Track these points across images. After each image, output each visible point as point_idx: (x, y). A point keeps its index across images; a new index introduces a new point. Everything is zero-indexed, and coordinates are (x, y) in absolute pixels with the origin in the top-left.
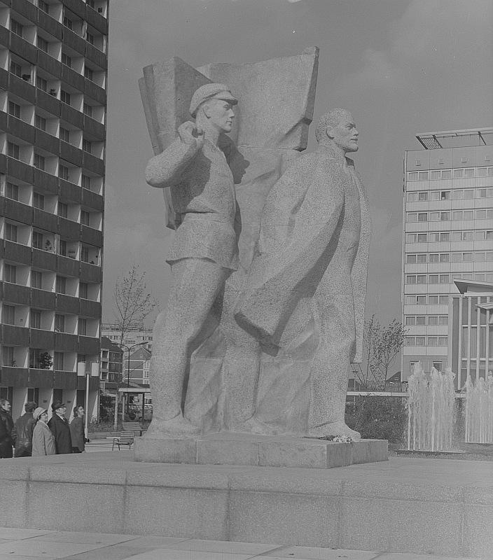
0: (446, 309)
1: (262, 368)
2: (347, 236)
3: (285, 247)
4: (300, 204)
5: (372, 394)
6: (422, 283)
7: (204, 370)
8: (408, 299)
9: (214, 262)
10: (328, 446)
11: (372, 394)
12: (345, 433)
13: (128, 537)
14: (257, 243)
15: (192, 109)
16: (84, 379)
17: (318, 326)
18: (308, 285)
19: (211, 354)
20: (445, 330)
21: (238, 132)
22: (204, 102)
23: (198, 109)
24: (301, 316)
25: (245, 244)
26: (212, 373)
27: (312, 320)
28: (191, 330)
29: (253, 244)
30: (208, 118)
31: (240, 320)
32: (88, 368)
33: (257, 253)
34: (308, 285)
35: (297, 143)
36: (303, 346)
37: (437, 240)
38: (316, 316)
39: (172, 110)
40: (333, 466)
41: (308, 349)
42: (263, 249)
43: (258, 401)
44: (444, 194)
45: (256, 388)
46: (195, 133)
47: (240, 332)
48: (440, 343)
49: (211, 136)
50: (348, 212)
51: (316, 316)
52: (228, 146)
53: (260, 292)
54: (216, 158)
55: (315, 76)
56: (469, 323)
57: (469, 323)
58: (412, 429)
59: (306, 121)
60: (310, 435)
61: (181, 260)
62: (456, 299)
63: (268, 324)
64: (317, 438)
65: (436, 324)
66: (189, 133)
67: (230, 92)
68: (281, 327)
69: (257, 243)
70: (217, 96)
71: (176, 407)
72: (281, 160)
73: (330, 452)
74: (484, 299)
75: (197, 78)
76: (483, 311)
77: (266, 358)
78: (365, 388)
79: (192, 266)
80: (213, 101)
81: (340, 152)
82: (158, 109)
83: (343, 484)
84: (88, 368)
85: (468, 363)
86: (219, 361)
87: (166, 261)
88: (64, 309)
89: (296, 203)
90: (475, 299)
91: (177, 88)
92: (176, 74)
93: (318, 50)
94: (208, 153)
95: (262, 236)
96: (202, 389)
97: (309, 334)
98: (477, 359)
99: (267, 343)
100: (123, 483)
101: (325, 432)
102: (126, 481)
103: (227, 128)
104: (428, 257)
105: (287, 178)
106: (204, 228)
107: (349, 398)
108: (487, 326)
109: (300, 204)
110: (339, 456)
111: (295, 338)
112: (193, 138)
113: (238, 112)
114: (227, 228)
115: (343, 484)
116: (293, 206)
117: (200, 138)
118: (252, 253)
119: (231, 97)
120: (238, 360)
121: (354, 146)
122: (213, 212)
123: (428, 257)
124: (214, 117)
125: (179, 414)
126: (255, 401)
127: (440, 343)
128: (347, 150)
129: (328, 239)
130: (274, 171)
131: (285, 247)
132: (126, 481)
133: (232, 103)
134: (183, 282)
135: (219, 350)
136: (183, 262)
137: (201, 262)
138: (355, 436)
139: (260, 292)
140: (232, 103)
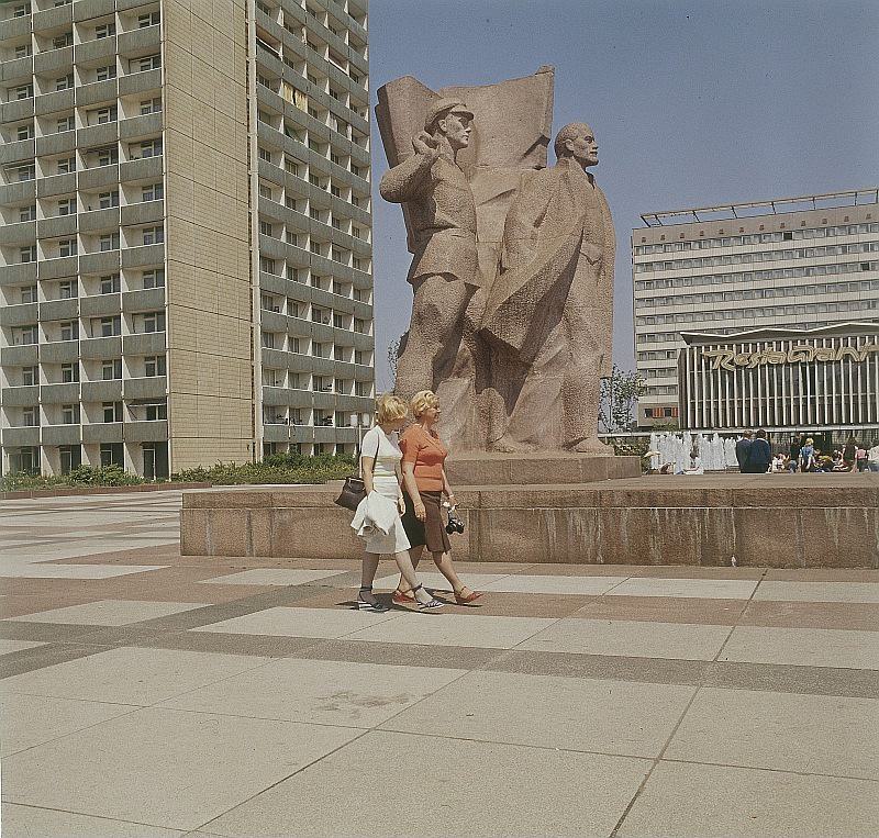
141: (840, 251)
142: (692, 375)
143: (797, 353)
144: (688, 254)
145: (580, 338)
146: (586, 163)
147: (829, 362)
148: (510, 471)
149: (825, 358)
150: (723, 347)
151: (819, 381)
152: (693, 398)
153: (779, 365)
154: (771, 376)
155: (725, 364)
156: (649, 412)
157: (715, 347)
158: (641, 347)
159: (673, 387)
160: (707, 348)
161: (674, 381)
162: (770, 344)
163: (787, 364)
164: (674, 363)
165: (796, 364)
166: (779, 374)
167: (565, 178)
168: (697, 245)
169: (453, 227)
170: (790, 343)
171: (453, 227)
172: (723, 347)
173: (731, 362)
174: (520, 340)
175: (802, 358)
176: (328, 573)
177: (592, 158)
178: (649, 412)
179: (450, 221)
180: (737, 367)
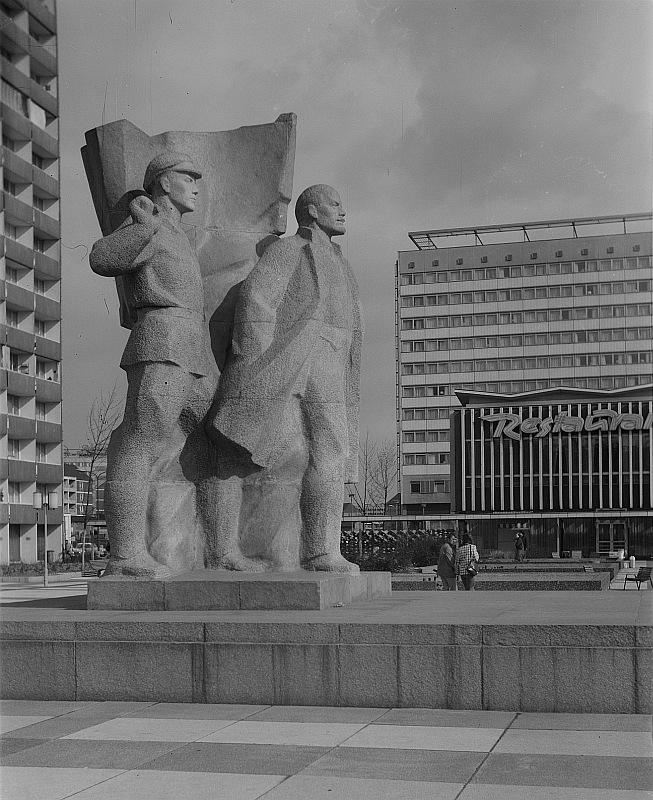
56: (601, 477)
57: (601, 477)
65: (413, 464)
141: (430, 392)
142: (468, 445)
143: (596, 420)
144: (491, 284)
145: (322, 440)
146: (332, 232)
147: (635, 431)
148: (242, 595)
149: (631, 427)
150: (506, 410)
151: (524, 451)
152: (468, 472)
153: (574, 433)
154: (565, 447)
155: (509, 430)
156: (415, 487)
157: (497, 411)
158: (407, 403)
159: (443, 432)
160: (487, 412)
161: (445, 446)
162: (565, 408)
163: (584, 432)
164: (445, 424)
165: (595, 433)
166: (575, 443)
167: (307, 250)
168: (408, 346)
169: (176, 306)
170: (589, 406)
171: (176, 306)
172: (506, 410)
173: (517, 429)
174: (20, 69)
175: (602, 425)
176: (36, 719)
177: (337, 226)
178: (415, 487)
179: (178, 303)
180: (525, 435)
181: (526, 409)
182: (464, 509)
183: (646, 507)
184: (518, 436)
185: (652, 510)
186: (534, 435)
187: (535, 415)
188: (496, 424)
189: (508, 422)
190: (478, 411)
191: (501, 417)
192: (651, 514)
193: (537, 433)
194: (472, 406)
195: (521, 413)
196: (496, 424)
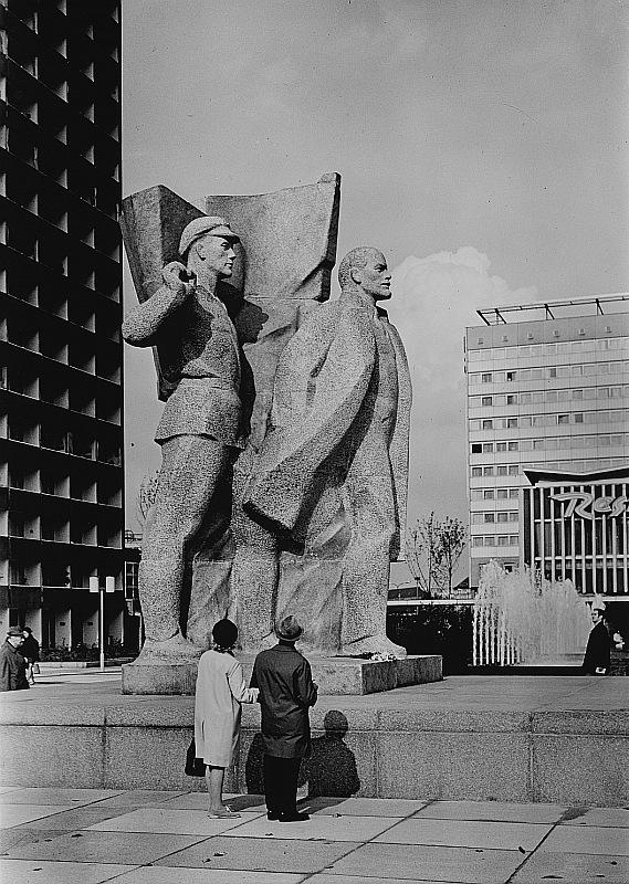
0: (517, 504)
1: (282, 571)
2: (382, 403)
3: (302, 420)
4: (321, 364)
5: (436, 602)
6: (489, 475)
7: (208, 576)
8: (474, 494)
9: (214, 439)
10: (364, 667)
11: (436, 602)
12: (387, 650)
13: (109, 792)
14: (269, 415)
15: (182, 250)
16: (98, 595)
17: (349, 516)
18: (336, 466)
19: (217, 557)
20: (517, 527)
21: (244, 279)
22: (196, 240)
23: (189, 249)
24: (328, 502)
25: (257, 419)
26: (219, 580)
27: (342, 508)
28: (189, 526)
29: (265, 416)
30: (203, 259)
31: (251, 511)
32: (102, 584)
33: (270, 427)
34: (336, 466)
35: (318, 291)
36: (331, 543)
37: (504, 426)
38: (347, 505)
39: (158, 252)
40: (370, 690)
41: (336, 546)
42: (276, 421)
43: (278, 612)
44: (510, 375)
45: (275, 597)
46: (184, 276)
47: (252, 527)
48: (512, 543)
49: (205, 280)
50: (383, 373)
51: (347, 505)
52: (231, 292)
53: (274, 475)
54: (215, 308)
55: (336, 209)
56: (542, 516)
57: (542, 516)
58: (478, 636)
59: (327, 264)
60: (345, 652)
61: (173, 437)
62: (527, 492)
63: (287, 516)
64: (351, 656)
65: (506, 520)
66: (175, 276)
67: (228, 226)
68: (304, 516)
69: (269, 415)
70: (213, 232)
71: (172, 624)
72: (298, 313)
73: (366, 675)
74: (557, 491)
75: (189, 213)
76: (557, 504)
77: (287, 558)
78: (427, 596)
79: (186, 444)
80: (207, 239)
81: (367, 298)
82: (141, 251)
83: (379, 714)
84: (102, 584)
85: (543, 563)
86: (227, 564)
87: (156, 440)
88: (83, 519)
89: (316, 363)
90: (547, 491)
91: (163, 224)
92: (161, 207)
93: (339, 177)
94: (202, 301)
95: (275, 405)
96: (206, 600)
97: (339, 527)
98: (552, 558)
99: (288, 540)
100: (103, 723)
101: (363, 648)
102: (105, 721)
103: (227, 271)
104: (495, 446)
105: (304, 333)
106: (204, 394)
107: (390, 609)
108: (562, 520)
109: (321, 364)
110: (379, 678)
111: (322, 532)
112: (181, 282)
113: (243, 253)
114: (229, 397)
115: (379, 714)
116: (312, 367)
117: (191, 282)
118: (264, 426)
119: (230, 233)
120: (249, 563)
121: (384, 292)
122: (212, 376)
123: (495, 446)
124: (209, 258)
125: (177, 632)
126: (274, 613)
127: (512, 543)
128: (377, 297)
129: (356, 406)
130: (289, 327)
131: (302, 420)
132: (105, 721)
133: (231, 241)
134: (176, 466)
135: (227, 550)
136: (175, 440)
137: (199, 439)
138: (398, 652)
139: (274, 475)
140: (231, 241)
155: (580, 511)
173: (588, 509)
180: (598, 514)
181: (598, 489)
182: (615, 591)
183: (621, 593)
184: (590, 516)
185: (628, 594)
186: (607, 514)
187: (608, 493)
188: (567, 503)
189: (579, 501)
190: (547, 491)
191: (573, 496)
192: (626, 599)
193: (611, 512)
194: (541, 485)
195: (593, 491)
196: (567, 503)
